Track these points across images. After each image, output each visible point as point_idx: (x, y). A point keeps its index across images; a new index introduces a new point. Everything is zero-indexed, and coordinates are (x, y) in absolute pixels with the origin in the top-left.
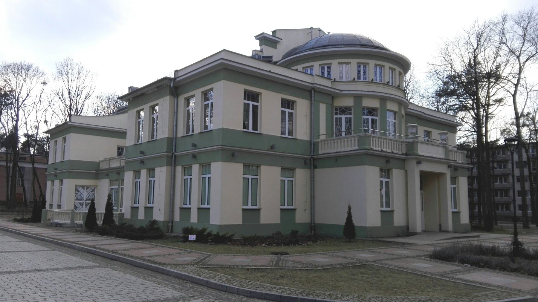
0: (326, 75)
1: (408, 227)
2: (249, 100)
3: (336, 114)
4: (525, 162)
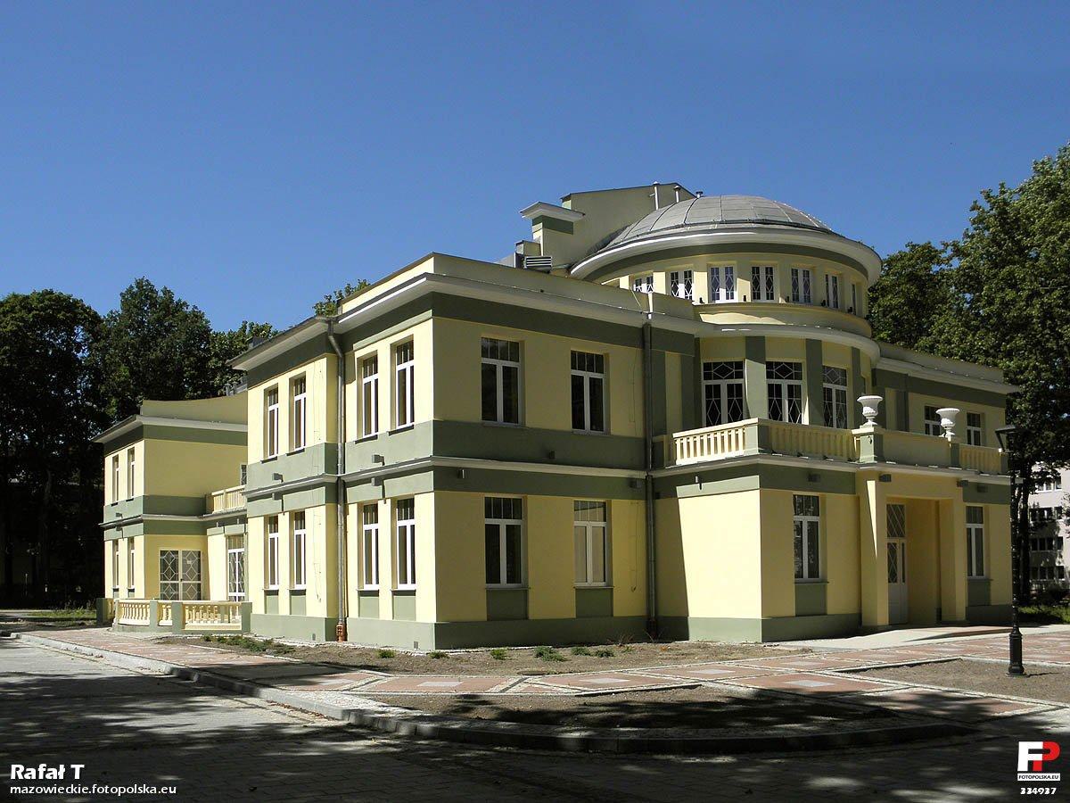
0: (801, 294)
1: (860, 615)
2: (582, 369)
3: (707, 377)
4: (78, 324)
